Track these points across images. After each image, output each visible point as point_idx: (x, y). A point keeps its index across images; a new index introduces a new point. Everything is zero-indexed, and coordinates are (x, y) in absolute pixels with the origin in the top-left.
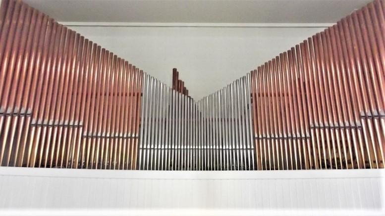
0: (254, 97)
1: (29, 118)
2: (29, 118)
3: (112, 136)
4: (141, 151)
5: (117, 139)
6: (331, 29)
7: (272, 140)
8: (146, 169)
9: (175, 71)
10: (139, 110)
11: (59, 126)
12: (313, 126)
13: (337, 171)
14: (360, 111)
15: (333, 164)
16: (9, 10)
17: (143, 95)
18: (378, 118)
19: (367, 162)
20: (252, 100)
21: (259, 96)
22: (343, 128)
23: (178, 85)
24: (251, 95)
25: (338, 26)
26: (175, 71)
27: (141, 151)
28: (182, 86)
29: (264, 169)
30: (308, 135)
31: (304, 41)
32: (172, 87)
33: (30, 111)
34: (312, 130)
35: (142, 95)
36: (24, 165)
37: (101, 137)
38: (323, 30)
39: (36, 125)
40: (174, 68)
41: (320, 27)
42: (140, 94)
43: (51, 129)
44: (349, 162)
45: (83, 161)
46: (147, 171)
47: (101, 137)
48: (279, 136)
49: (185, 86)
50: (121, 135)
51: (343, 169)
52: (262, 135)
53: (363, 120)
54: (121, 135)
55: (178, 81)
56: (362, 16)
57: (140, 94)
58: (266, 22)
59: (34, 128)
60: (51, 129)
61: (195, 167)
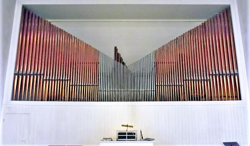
0: (156, 64)
1: (42, 77)
2: (42, 77)
3: (85, 84)
4: (99, 92)
5: (87, 86)
6: (198, 27)
7: (165, 86)
8: (102, 101)
9: (116, 48)
10: (98, 68)
11: (57, 80)
12: (188, 79)
13: (196, 102)
14: (210, 71)
15: (197, 98)
16: (26, 18)
17: (100, 63)
18: (226, 75)
19: (211, 97)
20: (155, 65)
21: (159, 63)
22: (233, 75)
23: (118, 57)
24: (155, 63)
25: (208, 21)
26: (116, 48)
27: (99, 92)
28: (120, 57)
29: (160, 101)
30: (182, 84)
31: (190, 30)
32: (114, 59)
33: (42, 73)
34: (185, 81)
35: (99, 63)
36: (42, 100)
37: (65, 80)
38: (201, 24)
39: (46, 80)
40: (116, 46)
41: (198, 23)
42: (98, 63)
43: (53, 82)
44: (202, 97)
45: (76, 97)
46: (103, 102)
47: (65, 80)
48: (198, 78)
49: (121, 56)
50: (89, 84)
51: (197, 101)
52: (164, 84)
53: (211, 77)
54: (89, 84)
55: (118, 53)
56: (226, 14)
57: (98, 63)
58: (166, 19)
59: (45, 82)
60: (32, 77)
61: (120, 100)
